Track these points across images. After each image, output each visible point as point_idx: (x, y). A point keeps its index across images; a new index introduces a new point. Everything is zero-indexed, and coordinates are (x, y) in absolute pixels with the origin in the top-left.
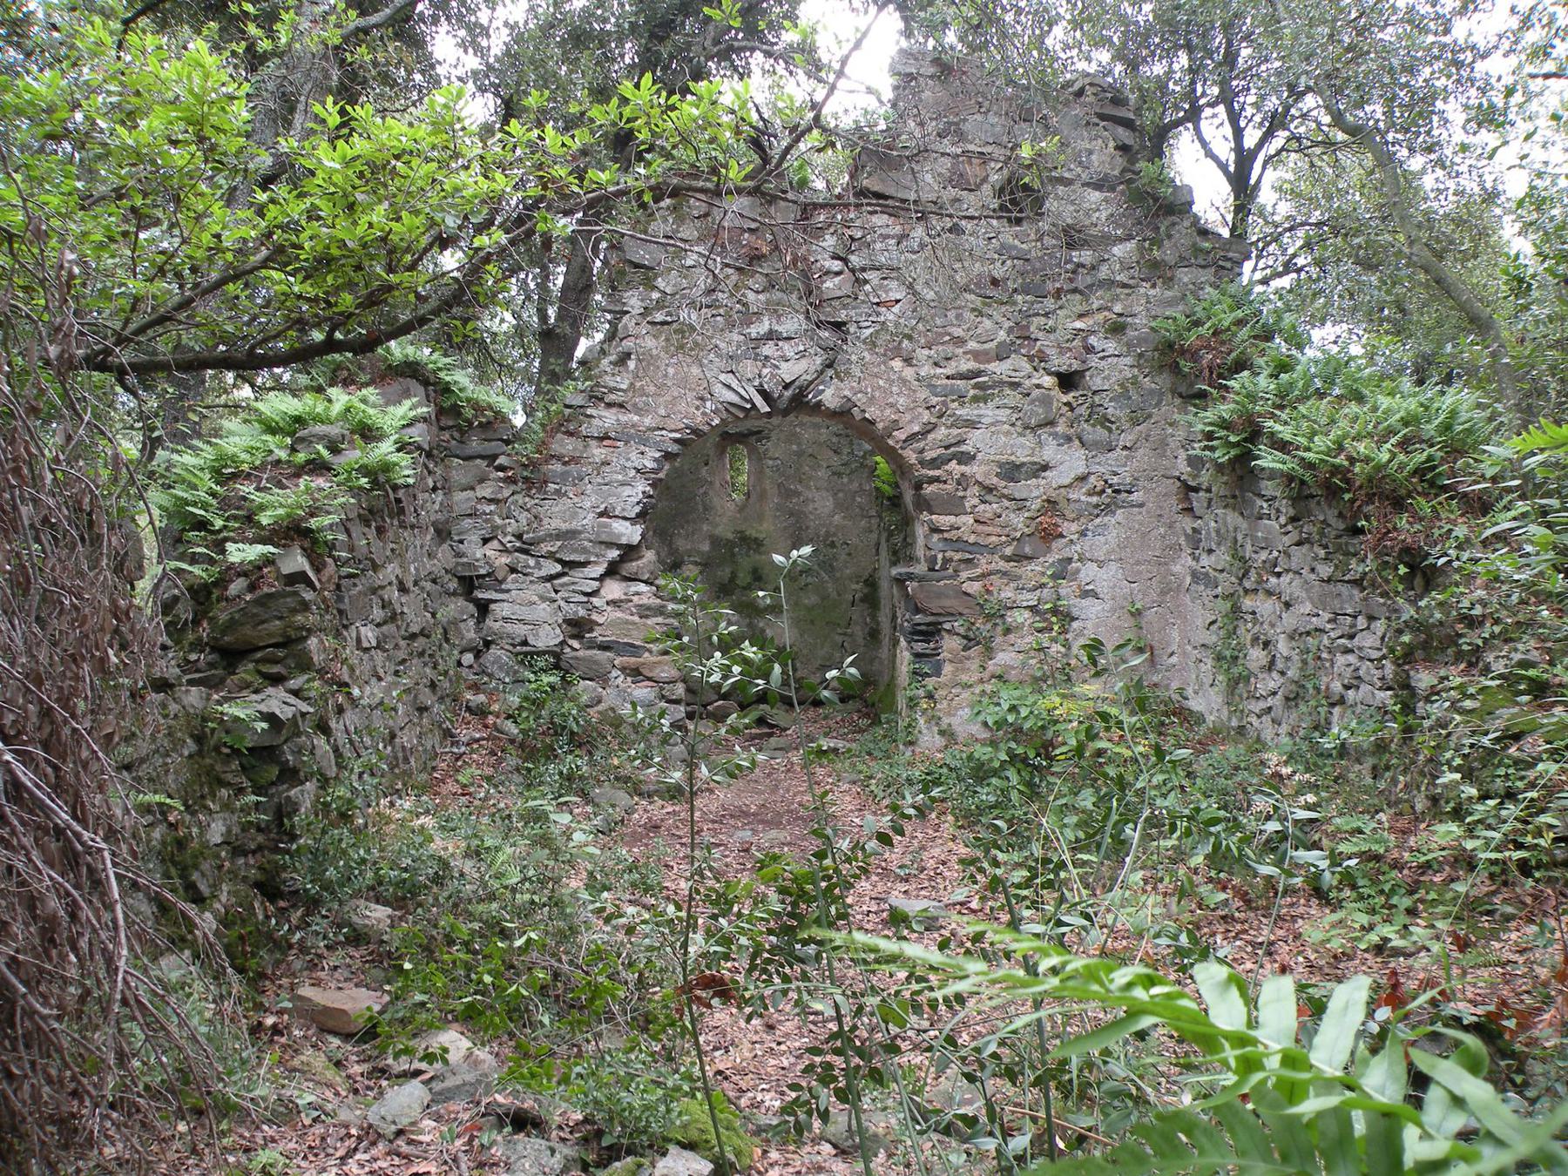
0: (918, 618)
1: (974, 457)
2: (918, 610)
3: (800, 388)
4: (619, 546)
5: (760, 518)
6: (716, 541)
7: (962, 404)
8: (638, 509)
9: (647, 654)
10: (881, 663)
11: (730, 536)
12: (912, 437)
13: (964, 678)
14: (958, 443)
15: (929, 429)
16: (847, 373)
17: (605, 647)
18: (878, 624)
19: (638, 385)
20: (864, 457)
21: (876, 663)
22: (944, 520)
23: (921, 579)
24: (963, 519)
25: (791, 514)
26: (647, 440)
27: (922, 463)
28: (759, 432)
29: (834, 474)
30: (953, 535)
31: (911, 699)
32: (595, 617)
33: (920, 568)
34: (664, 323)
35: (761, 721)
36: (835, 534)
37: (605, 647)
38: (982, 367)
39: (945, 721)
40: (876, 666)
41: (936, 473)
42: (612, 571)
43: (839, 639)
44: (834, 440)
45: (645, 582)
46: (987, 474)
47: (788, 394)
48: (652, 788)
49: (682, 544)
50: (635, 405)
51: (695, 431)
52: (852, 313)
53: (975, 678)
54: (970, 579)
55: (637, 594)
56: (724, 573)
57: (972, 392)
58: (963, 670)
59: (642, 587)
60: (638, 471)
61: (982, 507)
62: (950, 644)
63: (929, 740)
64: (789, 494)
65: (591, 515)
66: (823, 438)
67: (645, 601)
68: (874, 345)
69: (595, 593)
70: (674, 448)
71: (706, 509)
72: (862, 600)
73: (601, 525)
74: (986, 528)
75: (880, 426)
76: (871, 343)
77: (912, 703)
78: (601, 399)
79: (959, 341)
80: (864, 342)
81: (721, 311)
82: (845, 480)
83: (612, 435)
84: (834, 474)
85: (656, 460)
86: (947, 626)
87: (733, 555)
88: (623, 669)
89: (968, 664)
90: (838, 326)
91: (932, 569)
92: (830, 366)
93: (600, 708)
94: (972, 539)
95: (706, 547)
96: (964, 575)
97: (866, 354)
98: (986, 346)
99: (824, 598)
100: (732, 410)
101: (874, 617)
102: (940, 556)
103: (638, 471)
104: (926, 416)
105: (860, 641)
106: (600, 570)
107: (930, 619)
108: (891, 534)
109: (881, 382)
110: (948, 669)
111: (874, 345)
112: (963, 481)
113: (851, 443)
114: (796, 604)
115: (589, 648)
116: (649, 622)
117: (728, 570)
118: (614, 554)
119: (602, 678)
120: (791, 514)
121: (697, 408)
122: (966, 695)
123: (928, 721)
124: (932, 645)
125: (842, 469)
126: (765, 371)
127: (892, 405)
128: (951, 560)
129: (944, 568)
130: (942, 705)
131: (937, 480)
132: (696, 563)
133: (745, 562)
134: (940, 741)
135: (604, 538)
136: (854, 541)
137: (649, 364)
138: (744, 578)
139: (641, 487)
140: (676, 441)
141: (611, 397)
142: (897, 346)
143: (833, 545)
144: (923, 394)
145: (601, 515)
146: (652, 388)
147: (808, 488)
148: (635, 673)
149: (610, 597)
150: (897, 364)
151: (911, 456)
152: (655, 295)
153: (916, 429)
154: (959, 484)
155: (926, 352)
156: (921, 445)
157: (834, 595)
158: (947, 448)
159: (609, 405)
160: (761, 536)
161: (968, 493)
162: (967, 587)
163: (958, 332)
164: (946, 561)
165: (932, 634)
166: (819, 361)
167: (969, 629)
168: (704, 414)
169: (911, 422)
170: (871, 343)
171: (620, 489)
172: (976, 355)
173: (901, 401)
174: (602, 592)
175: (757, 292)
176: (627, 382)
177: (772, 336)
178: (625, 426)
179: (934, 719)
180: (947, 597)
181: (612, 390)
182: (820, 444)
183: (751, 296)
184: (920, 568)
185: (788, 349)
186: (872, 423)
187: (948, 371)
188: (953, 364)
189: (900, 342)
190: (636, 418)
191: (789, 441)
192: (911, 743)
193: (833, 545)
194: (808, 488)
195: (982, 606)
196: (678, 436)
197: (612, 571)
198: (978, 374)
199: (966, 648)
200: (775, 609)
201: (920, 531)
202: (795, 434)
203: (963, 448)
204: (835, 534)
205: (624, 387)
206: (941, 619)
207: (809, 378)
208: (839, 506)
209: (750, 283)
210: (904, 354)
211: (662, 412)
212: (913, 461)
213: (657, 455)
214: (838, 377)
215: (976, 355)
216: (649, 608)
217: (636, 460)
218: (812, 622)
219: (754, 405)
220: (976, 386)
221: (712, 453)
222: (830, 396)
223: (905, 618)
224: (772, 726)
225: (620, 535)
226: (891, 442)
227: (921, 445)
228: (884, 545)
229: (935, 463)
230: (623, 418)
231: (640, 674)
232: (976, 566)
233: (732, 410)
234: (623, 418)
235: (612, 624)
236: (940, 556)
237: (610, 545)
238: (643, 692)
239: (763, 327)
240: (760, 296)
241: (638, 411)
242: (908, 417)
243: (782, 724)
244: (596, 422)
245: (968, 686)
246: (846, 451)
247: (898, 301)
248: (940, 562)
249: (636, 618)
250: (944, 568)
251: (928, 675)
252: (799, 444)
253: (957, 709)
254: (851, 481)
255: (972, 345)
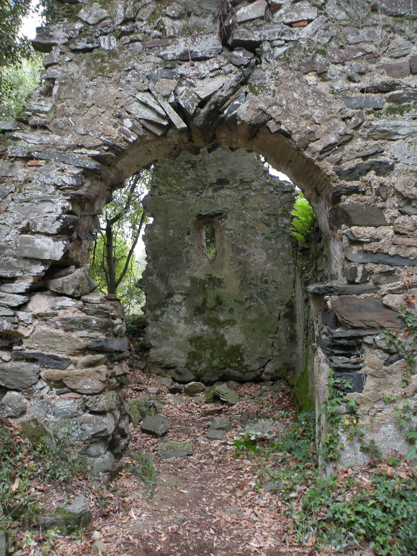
0: (338, 332)
1: (392, 168)
2: (337, 323)
3: (216, 103)
4: (44, 262)
5: (222, 267)
6: (194, 281)
7: (378, 116)
8: (58, 225)
9: (71, 367)
10: (297, 356)
11: (203, 277)
12: (329, 148)
13: (387, 393)
14: (376, 154)
15: (346, 139)
16: (262, 86)
17: (32, 359)
18: (295, 331)
19: (59, 106)
20: (285, 228)
21: (294, 356)
22: (363, 232)
23: (341, 292)
24: (384, 230)
25: (240, 263)
26: (67, 157)
27: (339, 173)
28: (220, 214)
29: (266, 238)
30: (372, 247)
31: (333, 415)
32: (21, 330)
33: (341, 282)
34: (86, 50)
35: (216, 398)
36: (267, 275)
37: (32, 359)
38: (397, 81)
39: (368, 437)
40: (294, 358)
41: (355, 183)
42: (40, 287)
43: (270, 341)
44: (266, 218)
45: (72, 297)
46: (406, 185)
47: (203, 111)
48: (48, 519)
49: (174, 283)
50: (56, 125)
51: (112, 147)
52: (266, 33)
53: (399, 392)
54: (391, 292)
55: (63, 308)
56: (199, 300)
57: (387, 105)
58: (385, 384)
59: (68, 302)
60: (58, 187)
61: (402, 218)
62: (371, 359)
63: (352, 457)
64: (238, 251)
65: (14, 232)
66: (259, 216)
67: (70, 315)
68: (288, 61)
69: (22, 307)
70: (92, 164)
71: (188, 261)
72: (285, 316)
73: (22, 241)
74: (405, 240)
75: (296, 137)
76: (285, 60)
77: (333, 418)
78: (26, 123)
79: (372, 57)
80: (278, 59)
81: (140, 36)
82: (273, 242)
83: (35, 154)
84: (266, 238)
85: (75, 176)
86: (368, 340)
87: (204, 289)
88: (48, 381)
89: (390, 378)
90: (252, 47)
91: (351, 282)
92: (244, 83)
93: (24, 419)
94: (392, 251)
95: (188, 284)
96: (385, 288)
97: (280, 69)
98: (399, 61)
99: (261, 315)
100: (149, 127)
101: (292, 327)
102: (360, 269)
103: (58, 187)
104: (342, 127)
105: (284, 342)
106: (23, 285)
107: (351, 333)
108: (303, 273)
109: (296, 95)
110: (369, 383)
111: (288, 61)
112: (382, 192)
113: (277, 219)
114: (244, 319)
115: (16, 360)
116: (74, 335)
117: (201, 298)
118: (39, 269)
119: (28, 390)
120: (240, 263)
121: (115, 126)
122: (388, 410)
123: (350, 438)
124: (353, 359)
125: (271, 235)
126: (181, 89)
127: (307, 117)
128: (371, 273)
129: (364, 281)
130: (365, 421)
131: (356, 190)
132: (182, 294)
133: (211, 294)
134: (362, 459)
135: (27, 253)
136: (279, 279)
137: (71, 87)
138: (211, 303)
139: (61, 203)
140: (95, 158)
141: (36, 119)
142: (309, 62)
143: (266, 282)
144: (338, 106)
145: (25, 230)
146: (72, 109)
147: (250, 247)
148: (59, 384)
149: (37, 311)
150: (311, 78)
151: (328, 166)
152: (78, 26)
153: (333, 139)
154: (378, 194)
155: (340, 68)
156: (339, 155)
157: (267, 313)
158: (365, 158)
159: (35, 127)
160: (222, 277)
161: (388, 204)
162: (389, 300)
163: (370, 48)
164: (367, 273)
165: (353, 348)
166: (233, 77)
167: (391, 342)
168: (121, 131)
169: (327, 132)
170: (285, 60)
171: (41, 205)
172: (389, 69)
173: (317, 112)
174: (30, 306)
175: (174, 18)
176: (50, 105)
177: (186, 57)
178: (47, 146)
179: (357, 436)
180: (369, 310)
181: (35, 113)
182: (257, 220)
183: (168, 22)
184: (341, 282)
185: (203, 68)
186: (287, 135)
187: (364, 84)
188: (367, 78)
189: (313, 58)
190: (57, 138)
191: (238, 218)
192: (332, 460)
193: (266, 282)
194: (250, 247)
195: (403, 319)
196: (96, 152)
197: (40, 287)
198: (392, 87)
199: (388, 363)
200: (231, 322)
201: (336, 249)
202: (242, 215)
203: (382, 159)
204: (267, 275)
205: (47, 109)
206: (362, 333)
207: (224, 94)
208: (269, 258)
209: (168, 11)
210: (318, 68)
211: (82, 131)
212: (331, 172)
213: (76, 171)
214: (252, 90)
215: (389, 69)
216: (73, 322)
217: (55, 177)
218: (253, 330)
219: (170, 121)
220: (389, 100)
221: (191, 227)
222: (244, 109)
223: (321, 330)
224: (223, 403)
225: (43, 251)
226: (307, 154)
227: (339, 155)
228: (298, 280)
229: (352, 174)
230: (46, 139)
231: (65, 386)
232: (397, 279)
233: (149, 127)
234: (46, 139)
235: (38, 337)
236: (360, 269)
237: (35, 260)
238: (66, 403)
239: (180, 47)
240: (177, 22)
241: (60, 131)
242: (324, 127)
243: (230, 401)
244: (20, 143)
245: (390, 402)
246: (273, 224)
247: (309, 21)
248: (360, 274)
249: (61, 332)
250: (364, 281)
251: (349, 390)
252: (245, 220)
253: (379, 425)
254: (277, 242)
255: (385, 60)
